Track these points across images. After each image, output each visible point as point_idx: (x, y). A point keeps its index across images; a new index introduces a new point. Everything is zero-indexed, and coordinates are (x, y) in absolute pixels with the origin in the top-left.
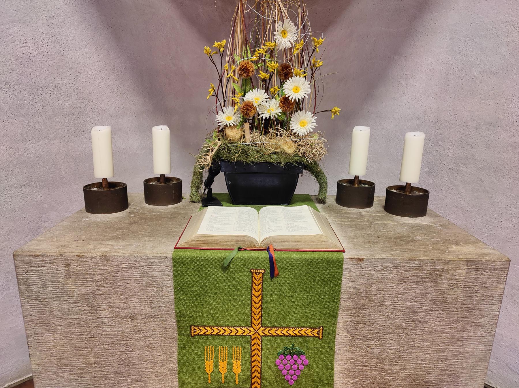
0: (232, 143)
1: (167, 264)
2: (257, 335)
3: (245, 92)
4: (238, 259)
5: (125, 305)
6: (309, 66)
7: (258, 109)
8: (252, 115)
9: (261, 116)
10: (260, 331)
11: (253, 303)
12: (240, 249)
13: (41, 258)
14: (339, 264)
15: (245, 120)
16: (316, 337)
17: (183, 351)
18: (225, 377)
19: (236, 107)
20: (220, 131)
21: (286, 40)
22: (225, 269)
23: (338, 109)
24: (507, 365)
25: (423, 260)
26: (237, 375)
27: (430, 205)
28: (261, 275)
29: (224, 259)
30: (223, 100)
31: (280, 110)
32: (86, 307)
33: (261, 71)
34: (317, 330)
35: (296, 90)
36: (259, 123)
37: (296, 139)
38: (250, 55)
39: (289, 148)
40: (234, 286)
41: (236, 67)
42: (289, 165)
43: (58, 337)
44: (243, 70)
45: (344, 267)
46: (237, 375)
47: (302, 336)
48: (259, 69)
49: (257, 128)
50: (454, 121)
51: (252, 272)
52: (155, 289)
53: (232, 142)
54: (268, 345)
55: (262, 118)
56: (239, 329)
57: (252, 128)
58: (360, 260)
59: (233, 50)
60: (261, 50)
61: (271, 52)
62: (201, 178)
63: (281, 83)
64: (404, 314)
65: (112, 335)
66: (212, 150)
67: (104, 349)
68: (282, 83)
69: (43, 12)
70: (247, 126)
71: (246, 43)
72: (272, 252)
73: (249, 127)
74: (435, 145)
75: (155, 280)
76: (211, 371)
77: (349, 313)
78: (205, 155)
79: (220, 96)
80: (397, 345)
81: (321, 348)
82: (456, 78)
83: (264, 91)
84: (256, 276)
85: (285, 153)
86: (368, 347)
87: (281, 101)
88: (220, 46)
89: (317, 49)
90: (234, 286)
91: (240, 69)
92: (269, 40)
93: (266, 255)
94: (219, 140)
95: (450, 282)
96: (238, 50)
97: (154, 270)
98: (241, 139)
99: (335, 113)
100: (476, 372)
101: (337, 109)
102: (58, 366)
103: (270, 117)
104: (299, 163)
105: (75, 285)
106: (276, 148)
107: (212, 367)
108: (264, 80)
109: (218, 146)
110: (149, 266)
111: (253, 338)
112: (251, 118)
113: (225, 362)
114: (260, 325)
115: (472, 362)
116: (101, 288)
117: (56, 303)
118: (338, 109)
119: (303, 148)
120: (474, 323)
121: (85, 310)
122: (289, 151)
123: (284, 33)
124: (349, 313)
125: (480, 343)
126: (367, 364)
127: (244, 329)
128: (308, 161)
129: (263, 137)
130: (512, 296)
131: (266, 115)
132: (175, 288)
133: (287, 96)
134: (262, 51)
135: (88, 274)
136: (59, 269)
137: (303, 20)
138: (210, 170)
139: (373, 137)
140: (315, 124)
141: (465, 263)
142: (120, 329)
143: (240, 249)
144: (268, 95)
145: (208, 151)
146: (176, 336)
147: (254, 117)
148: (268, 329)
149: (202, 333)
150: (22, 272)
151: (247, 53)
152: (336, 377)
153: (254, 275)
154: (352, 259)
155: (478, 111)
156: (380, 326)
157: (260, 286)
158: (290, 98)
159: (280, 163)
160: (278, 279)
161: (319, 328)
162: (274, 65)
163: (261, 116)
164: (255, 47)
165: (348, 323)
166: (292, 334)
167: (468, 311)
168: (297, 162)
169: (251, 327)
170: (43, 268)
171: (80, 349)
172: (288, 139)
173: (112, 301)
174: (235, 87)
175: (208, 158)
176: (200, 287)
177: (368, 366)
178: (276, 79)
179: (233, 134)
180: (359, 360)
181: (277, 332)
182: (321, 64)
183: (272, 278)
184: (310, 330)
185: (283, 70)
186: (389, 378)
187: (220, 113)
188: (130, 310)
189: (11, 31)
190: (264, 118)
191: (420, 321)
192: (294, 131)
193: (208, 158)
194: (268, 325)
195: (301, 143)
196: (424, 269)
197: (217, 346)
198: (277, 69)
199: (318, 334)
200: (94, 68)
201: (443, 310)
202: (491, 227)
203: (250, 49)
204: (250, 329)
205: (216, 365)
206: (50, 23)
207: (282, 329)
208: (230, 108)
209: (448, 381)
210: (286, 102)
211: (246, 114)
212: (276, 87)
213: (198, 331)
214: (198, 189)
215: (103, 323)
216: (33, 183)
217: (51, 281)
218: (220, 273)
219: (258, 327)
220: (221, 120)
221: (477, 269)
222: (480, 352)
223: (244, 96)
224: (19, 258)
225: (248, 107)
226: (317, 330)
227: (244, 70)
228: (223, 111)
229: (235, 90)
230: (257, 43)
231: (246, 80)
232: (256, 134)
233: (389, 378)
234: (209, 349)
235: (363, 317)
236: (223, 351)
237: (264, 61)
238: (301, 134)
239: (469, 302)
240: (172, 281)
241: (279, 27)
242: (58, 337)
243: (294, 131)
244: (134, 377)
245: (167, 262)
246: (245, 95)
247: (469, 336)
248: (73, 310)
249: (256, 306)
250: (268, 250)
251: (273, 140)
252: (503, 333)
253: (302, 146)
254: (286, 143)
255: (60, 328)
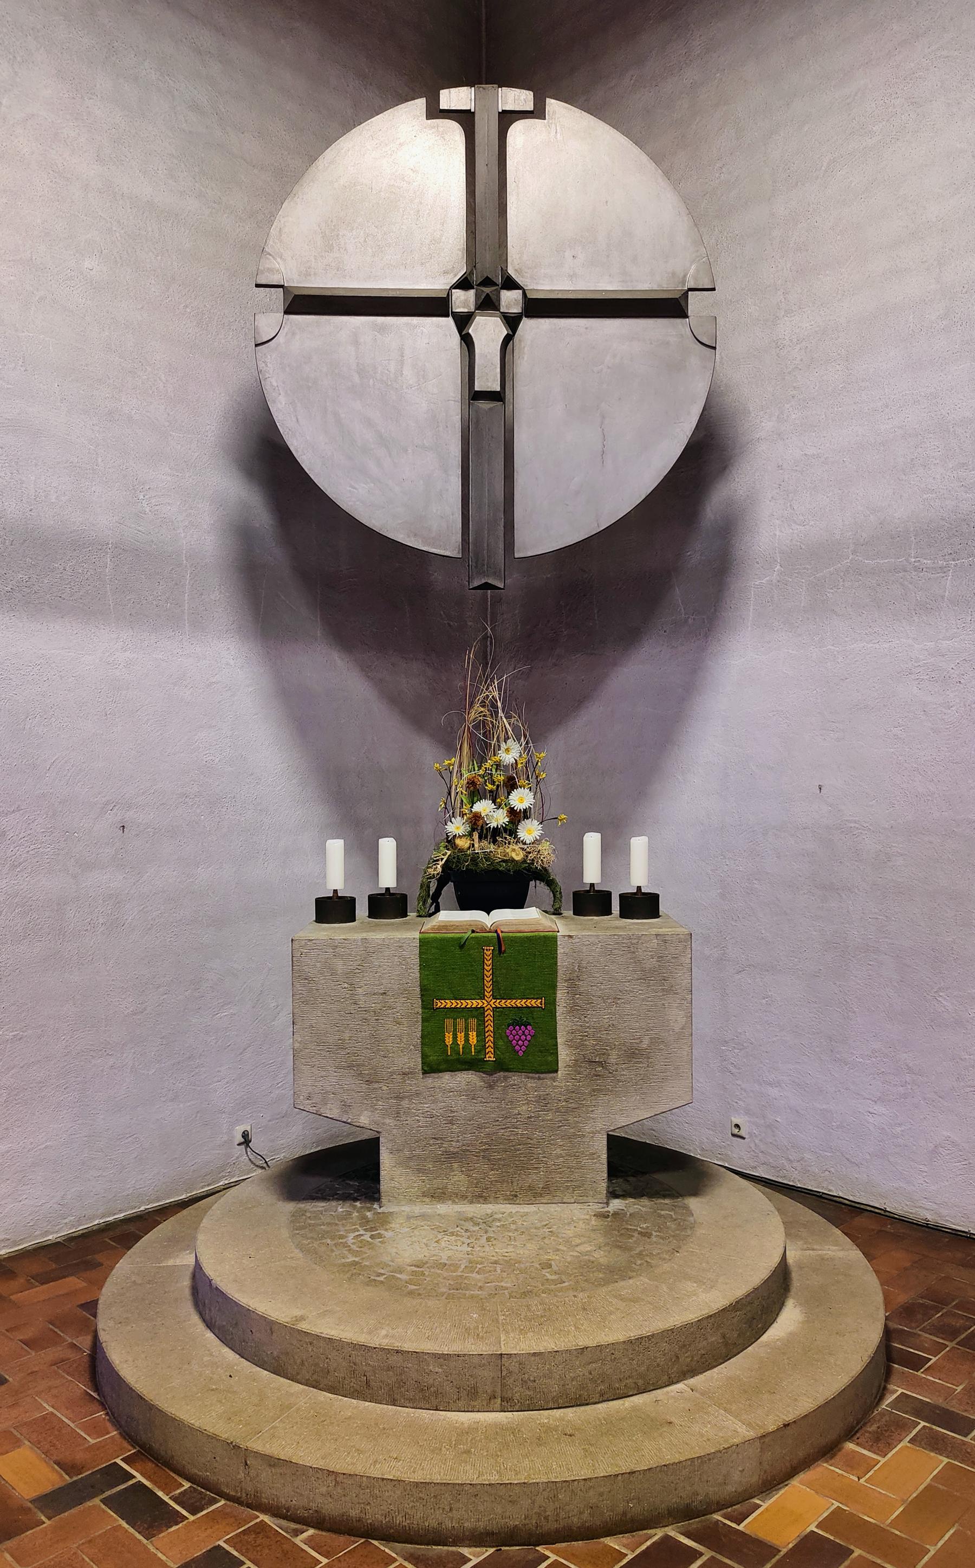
0: (462, 852)
1: (414, 945)
2: (489, 1006)
3: (473, 803)
4: (472, 938)
5: (378, 982)
6: (534, 777)
7: (486, 819)
8: (481, 825)
9: (489, 825)
10: (492, 1003)
11: (485, 977)
12: (473, 931)
13: (314, 941)
14: (554, 939)
15: (473, 830)
16: (539, 1007)
17: (426, 1024)
18: (463, 1048)
19: (465, 817)
20: (448, 842)
21: (510, 756)
22: (462, 947)
23: (565, 816)
24: (843, 1155)
25: (621, 935)
26: (473, 1046)
27: (662, 909)
28: (491, 951)
29: (460, 938)
30: (452, 811)
31: (508, 820)
32: (346, 985)
33: (487, 784)
34: (539, 1001)
35: (521, 800)
36: (487, 832)
37: (523, 846)
38: (476, 769)
39: (517, 855)
40: (469, 962)
41: (464, 782)
42: (518, 873)
43: (320, 1014)
44: (471, 783)
45: (559, 943)
46: (473, 1046)
47: (527, 1007)
48: (486, 781)
49: (486, 837)
50: (740, 825)
51: (484, 949)
52: (404, 967)
53: (461, 850)
54: (499, 1016)
55: (490, 827)
56: (474, 1001)
57: (480, 838)
58: (570, 937)
59: (460, 766)
60: (488, 764)
61: (498, 766)
62: (429, 890)
63: (508, 792)
64: (612, 984)
65: (365, 1011)
66: (442, 859)
67: (359, 1024)
68: (509, 794)
69: (229, 713)
70: (476, 836)
71: (472, 756)
72: (499, 932)
73: (477, 836)
74: (725, 858)
75: (405, 959)
76: (450, 1043)
77: (566, 985)
78: (435, 865)
79: (449, 808)
80: (609, 1014)
81: (544, 1018)
82: (734, 773)
83: (491, 802)
84: (487, 952)
85: (513, 860)
86: (585, 1017)
87: (508, 811)
88: (450, 764)
89: (539, 764)
90: (469, 962)
91: (468, 783)
92: (495, 755)
93: (496, 935)
94: (448, 850)
95: (646, 953)
96: (465, 764)
97: (404, 950)
98: (469, 848)
99: (561, 820)
100: (682, 1039)
101: (563, 816)
102: (317, 1043)
103: (497, 826)
104: (529, 869)
105: (339, 966)
106: (505, 856)
107: (451, 1039)
108: (491, 791)
109: (447, 856)
110: (400, 947)
111: (486, 1009)
112: (479, 828)
113: (463, 1034)
114: (491, 998)
115: (677, 1030)
116: (359, 967)
117: (323, 982)
118: (565, 816)
119: (531, 855)
120: (670, 991)
121: (345, 988)
122: (517, 858)
123: (507, 750)
124: (566, 985)
125: (680, 1010)
126: (586, 1034)
127: (478, 1001)
128: (537, 868)
129: (492, 846)
130: (832, 1051)
131: (493, 824)
132: (420, 965)
133: (512, 806)
134: (488, 765)
135: (350, 955)
136: (327, 951)
137: (525, 737)
138: (439, 880)
139: (652, 852)
140: (541, 832)
141: (655, 936)
142: (373, 1005)
143: (473, 931)
144: (495, 805)
145: (438, 860)
146: (420, 1010)
147: (482, 827)
148: (498, 1001)
149: (442, 1006)
150: (297, 954)
151: (474, 767)
152: (560, 1047)
153: (485, 951)
154: (564, 936)
155: (762, 813)
156: (593, 996)
157: (491, 961)
158: (515, 808)
159: (509, 871)
160: (505, 955)
161: (542, 999)
162: (500, 778)
163: (489, 825)
164: (481, 763)
165: (566, 995)
166: (519, 1005)
167: (664, 980)
168: (526, 870)
169: (484, 999)
170: (315, 950)
171: (338, 1025)
172: (516, 847)
173: (368, 979)
174: (463, 799)
175: (439, 866)
176: (441, 963)
177: (587, 1036)
178: (502, 791)
179: (462, 843)
180: (579, 1030)
181: (506, 1003)
182: (544, 776)
183: (500, 954)
184: (534, 1001)
185: (508, 782)
186: (607, 1048)
187: (449, 823)
188: (382, 987)
189: (197, 737)
190: (492, 827)
191: (626, 991)
192: (521, 839)
193: (439, 866)
194: (498, 997)
195: (528, 850)
196: (623, 943)
197: (455, 1019)
198: (503, 780)
199: (541, 1004)
200: (276, 771)
201: (644, 979)
202: (796, 960)
203: (477, 763)
204: (483, 1001)
205: (455, 1037)
206: (234, 724)
207: (510, 1001)
208: (459, 818)
209: (660, 1049)
210: (512, 812)
211: (475, 824)
212: (503, 798)
213: (439, 1004)
214: (425, 902)
215: (359, 999)
216: (200, 918)
217: (320, 962)
218: (458, 951)
219: (490, 999)
220: (450, 830)
221: (665, 941)
222: (682, 1020)
223: (472, 807)
224: (296, 942)
225: (477, 817)
226: (539, 1001)
227: (471, 783)
228: (451, 821)
229: (462, 801)
230: (482, 760)
231: (473, 792)
232: (485, 843)
233: (607, 1048)
234: (449, 1022)
235: (578, 987)
236: (461, 1023)
237: (491, 774)
238: (528, 842)
239: (664, 971)
240: (418, 960)
241: (503, 746)
242: (320, 1014)
243: (521, 839)
244: (382, 1053)
245: (415, 942)
246: (473, 806)
247: (669, 1003)
248: (335, 987)
249: (487, 979)
250: (496, 932)
251: (501, 848)
252: (832, 1107)
253: (530, 853)
254: (514, 850)
255: (323, 1005)
